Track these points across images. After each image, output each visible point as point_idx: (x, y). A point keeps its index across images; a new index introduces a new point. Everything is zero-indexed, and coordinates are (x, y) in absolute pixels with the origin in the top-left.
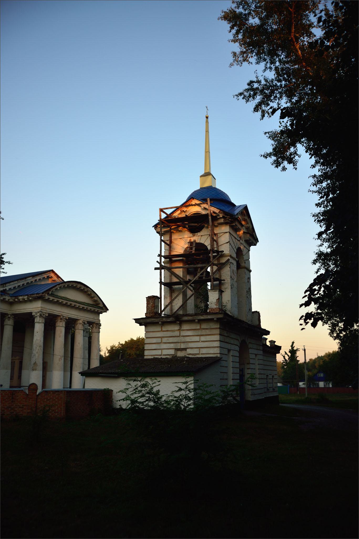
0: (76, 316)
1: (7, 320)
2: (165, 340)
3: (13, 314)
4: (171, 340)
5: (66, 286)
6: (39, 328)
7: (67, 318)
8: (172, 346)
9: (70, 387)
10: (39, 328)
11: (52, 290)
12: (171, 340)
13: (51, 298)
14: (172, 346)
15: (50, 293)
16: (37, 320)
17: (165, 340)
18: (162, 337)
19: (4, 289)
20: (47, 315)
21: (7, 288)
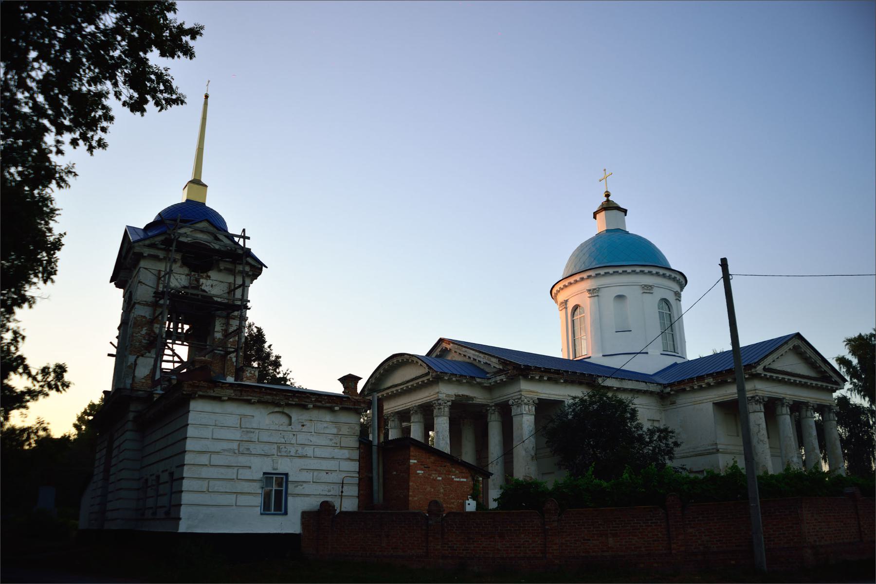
0: (547, 395)
3: (496, 405)
7: (537, 402)
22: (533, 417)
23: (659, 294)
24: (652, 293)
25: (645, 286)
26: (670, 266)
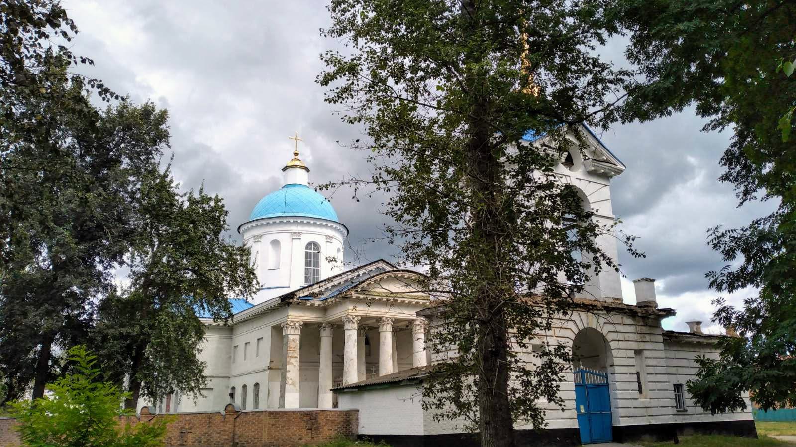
1: (322, 330)
5: (385, 277)
6: (352, 336)
9: (282, 405)
10: (352, 336)
11: (361, 286)
13: (362, 296)
15: (359, 290)
16: (348, 326)
19: (311, 291)
20: (360, 318)
22: (299, 336)
23: (306, 239)
24: (300, 239)
25: (295, 233)
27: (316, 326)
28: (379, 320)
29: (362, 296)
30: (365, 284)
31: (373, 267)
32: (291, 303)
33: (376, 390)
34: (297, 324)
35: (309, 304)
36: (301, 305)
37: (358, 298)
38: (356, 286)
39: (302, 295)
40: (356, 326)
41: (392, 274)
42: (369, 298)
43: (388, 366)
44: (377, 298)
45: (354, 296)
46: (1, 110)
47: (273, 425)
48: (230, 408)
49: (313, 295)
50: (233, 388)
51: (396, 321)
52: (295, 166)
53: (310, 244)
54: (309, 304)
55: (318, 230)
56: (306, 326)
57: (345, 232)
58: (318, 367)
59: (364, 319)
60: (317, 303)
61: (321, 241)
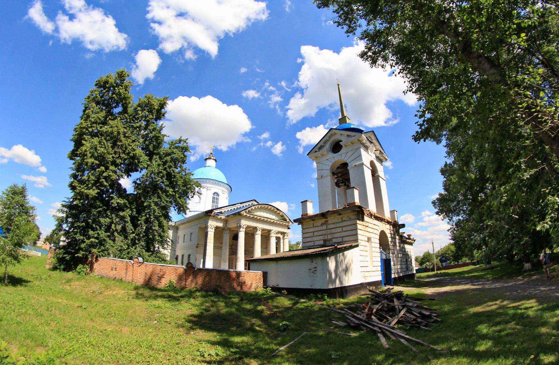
2: (316, 234)
4: (321, 233)
8: (321, 237)
11: (248, 209)
12: (321, 233)
13: (248, 215)
14: (321, 237)
15: (247, 211)
17: (316, 234)
18: (313, 232)
21: (223, 211)
26: (312, 145)
27: (221, 229)
28: (255, 229)
29: (248, 215)
30: (250, 209)
31: (250, 203)
32: (210, 215)
33: (297, 260)
34: (213, 227)
35: (219, 217)
36: (215, 217)
37: (246, 216)
38: (246, 209)
39: (216, 212)
40: (244, 230)
41: (256, 207)
42: (252, 216)
43: (273, 252)
44: (256, 217)
45: (245, 214)
46: (558, 105)
47: (218, 279)
48: (189, 265)
49: (221, 213)
50: (177, 256)
51: (263, 230)
52: (210, 158)
53: (215, 193)
54: (219, 217)
55: (219, 187)
56: (217, 228)
57: (230, 190)
58: (354, 232)
59: (248, 227)
60: (223, 217)
61: (220, 192)
